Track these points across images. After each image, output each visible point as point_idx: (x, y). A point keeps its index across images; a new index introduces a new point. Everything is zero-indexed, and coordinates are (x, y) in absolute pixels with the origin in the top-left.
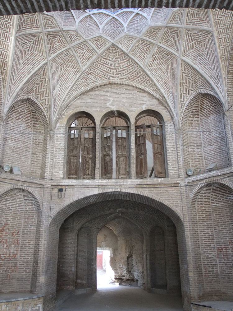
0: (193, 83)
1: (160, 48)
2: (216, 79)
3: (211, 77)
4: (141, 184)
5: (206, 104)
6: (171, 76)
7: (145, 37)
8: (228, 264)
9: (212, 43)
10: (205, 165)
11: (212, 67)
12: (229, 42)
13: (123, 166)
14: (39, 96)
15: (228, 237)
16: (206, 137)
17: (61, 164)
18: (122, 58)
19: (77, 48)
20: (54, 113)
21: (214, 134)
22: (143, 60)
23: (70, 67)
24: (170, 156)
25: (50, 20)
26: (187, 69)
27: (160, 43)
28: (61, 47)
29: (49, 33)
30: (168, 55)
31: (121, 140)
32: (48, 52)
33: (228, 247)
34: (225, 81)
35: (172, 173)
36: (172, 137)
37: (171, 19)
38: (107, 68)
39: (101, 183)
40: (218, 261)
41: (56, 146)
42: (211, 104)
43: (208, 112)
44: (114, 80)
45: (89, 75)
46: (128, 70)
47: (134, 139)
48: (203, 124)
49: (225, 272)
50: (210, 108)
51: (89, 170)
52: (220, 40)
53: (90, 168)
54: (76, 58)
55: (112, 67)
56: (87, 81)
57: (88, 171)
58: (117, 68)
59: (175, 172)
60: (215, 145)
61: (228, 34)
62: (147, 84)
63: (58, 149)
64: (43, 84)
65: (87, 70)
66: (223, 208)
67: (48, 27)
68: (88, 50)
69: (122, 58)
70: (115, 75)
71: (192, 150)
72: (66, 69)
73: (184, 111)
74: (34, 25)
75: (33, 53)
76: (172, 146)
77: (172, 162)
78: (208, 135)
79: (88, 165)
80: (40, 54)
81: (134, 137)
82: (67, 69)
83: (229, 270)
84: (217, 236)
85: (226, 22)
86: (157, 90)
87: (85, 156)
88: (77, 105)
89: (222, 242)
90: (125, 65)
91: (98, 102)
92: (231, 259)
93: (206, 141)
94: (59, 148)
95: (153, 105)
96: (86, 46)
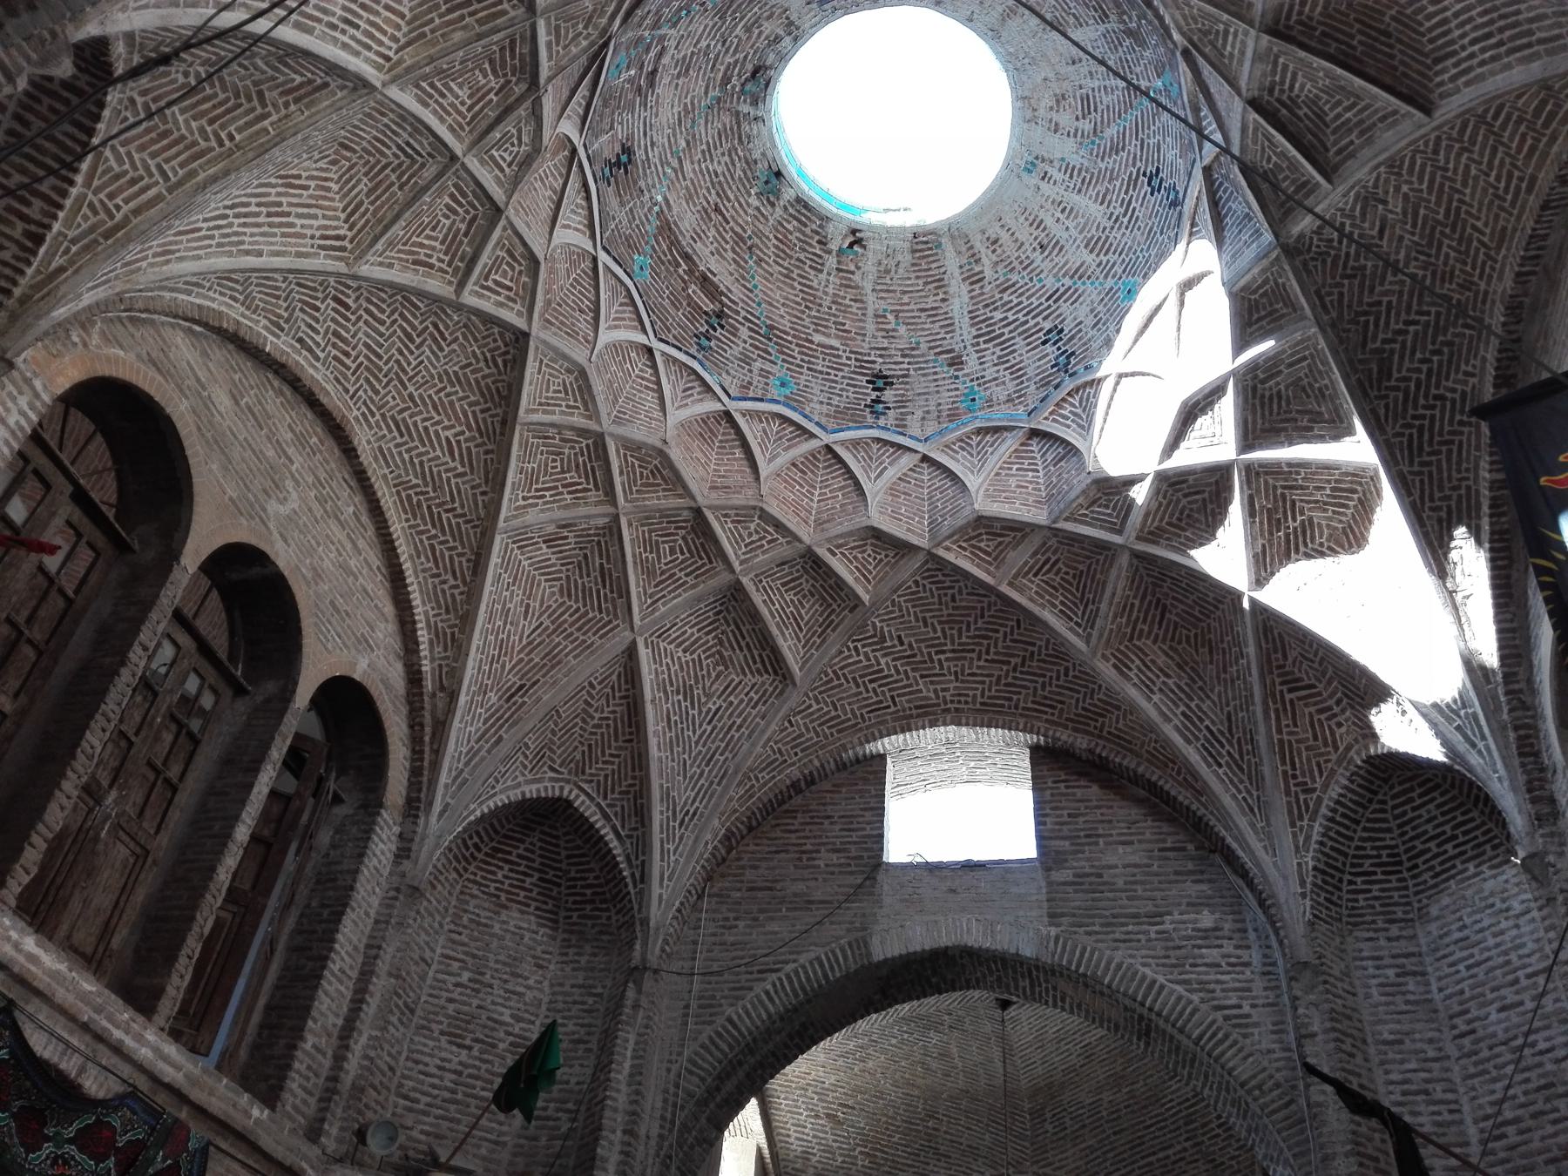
0: (580, 749)
3: (666, 796)
7: (618, 451)
9: (756, 704)
21: (493, 1003)
22: (524, 498)
25: (586, 27)
27: (630, 525)
28: (449, 114)
30: (604, 581)
34: (701, 855)
37: (732, 512)
38: (397, 361)
39: (32, 958)
43: (511, 885)
45: (333, 304)
46: (438, 458)
55: (410, 380)
58: (416, 405)
60: (475, 1052)
61: (818, 735)
62: (437, 580)
64: (229, 111)
67: (557, 28)
68: (455, 237)
70: (378, 417)
72: (326, 179)
80: (405, 29)
82: (331, 185)
86: (455, 643)
88: (167, 357)
90: (449, 433)
93: (443, 1008)
96: (474, 219)
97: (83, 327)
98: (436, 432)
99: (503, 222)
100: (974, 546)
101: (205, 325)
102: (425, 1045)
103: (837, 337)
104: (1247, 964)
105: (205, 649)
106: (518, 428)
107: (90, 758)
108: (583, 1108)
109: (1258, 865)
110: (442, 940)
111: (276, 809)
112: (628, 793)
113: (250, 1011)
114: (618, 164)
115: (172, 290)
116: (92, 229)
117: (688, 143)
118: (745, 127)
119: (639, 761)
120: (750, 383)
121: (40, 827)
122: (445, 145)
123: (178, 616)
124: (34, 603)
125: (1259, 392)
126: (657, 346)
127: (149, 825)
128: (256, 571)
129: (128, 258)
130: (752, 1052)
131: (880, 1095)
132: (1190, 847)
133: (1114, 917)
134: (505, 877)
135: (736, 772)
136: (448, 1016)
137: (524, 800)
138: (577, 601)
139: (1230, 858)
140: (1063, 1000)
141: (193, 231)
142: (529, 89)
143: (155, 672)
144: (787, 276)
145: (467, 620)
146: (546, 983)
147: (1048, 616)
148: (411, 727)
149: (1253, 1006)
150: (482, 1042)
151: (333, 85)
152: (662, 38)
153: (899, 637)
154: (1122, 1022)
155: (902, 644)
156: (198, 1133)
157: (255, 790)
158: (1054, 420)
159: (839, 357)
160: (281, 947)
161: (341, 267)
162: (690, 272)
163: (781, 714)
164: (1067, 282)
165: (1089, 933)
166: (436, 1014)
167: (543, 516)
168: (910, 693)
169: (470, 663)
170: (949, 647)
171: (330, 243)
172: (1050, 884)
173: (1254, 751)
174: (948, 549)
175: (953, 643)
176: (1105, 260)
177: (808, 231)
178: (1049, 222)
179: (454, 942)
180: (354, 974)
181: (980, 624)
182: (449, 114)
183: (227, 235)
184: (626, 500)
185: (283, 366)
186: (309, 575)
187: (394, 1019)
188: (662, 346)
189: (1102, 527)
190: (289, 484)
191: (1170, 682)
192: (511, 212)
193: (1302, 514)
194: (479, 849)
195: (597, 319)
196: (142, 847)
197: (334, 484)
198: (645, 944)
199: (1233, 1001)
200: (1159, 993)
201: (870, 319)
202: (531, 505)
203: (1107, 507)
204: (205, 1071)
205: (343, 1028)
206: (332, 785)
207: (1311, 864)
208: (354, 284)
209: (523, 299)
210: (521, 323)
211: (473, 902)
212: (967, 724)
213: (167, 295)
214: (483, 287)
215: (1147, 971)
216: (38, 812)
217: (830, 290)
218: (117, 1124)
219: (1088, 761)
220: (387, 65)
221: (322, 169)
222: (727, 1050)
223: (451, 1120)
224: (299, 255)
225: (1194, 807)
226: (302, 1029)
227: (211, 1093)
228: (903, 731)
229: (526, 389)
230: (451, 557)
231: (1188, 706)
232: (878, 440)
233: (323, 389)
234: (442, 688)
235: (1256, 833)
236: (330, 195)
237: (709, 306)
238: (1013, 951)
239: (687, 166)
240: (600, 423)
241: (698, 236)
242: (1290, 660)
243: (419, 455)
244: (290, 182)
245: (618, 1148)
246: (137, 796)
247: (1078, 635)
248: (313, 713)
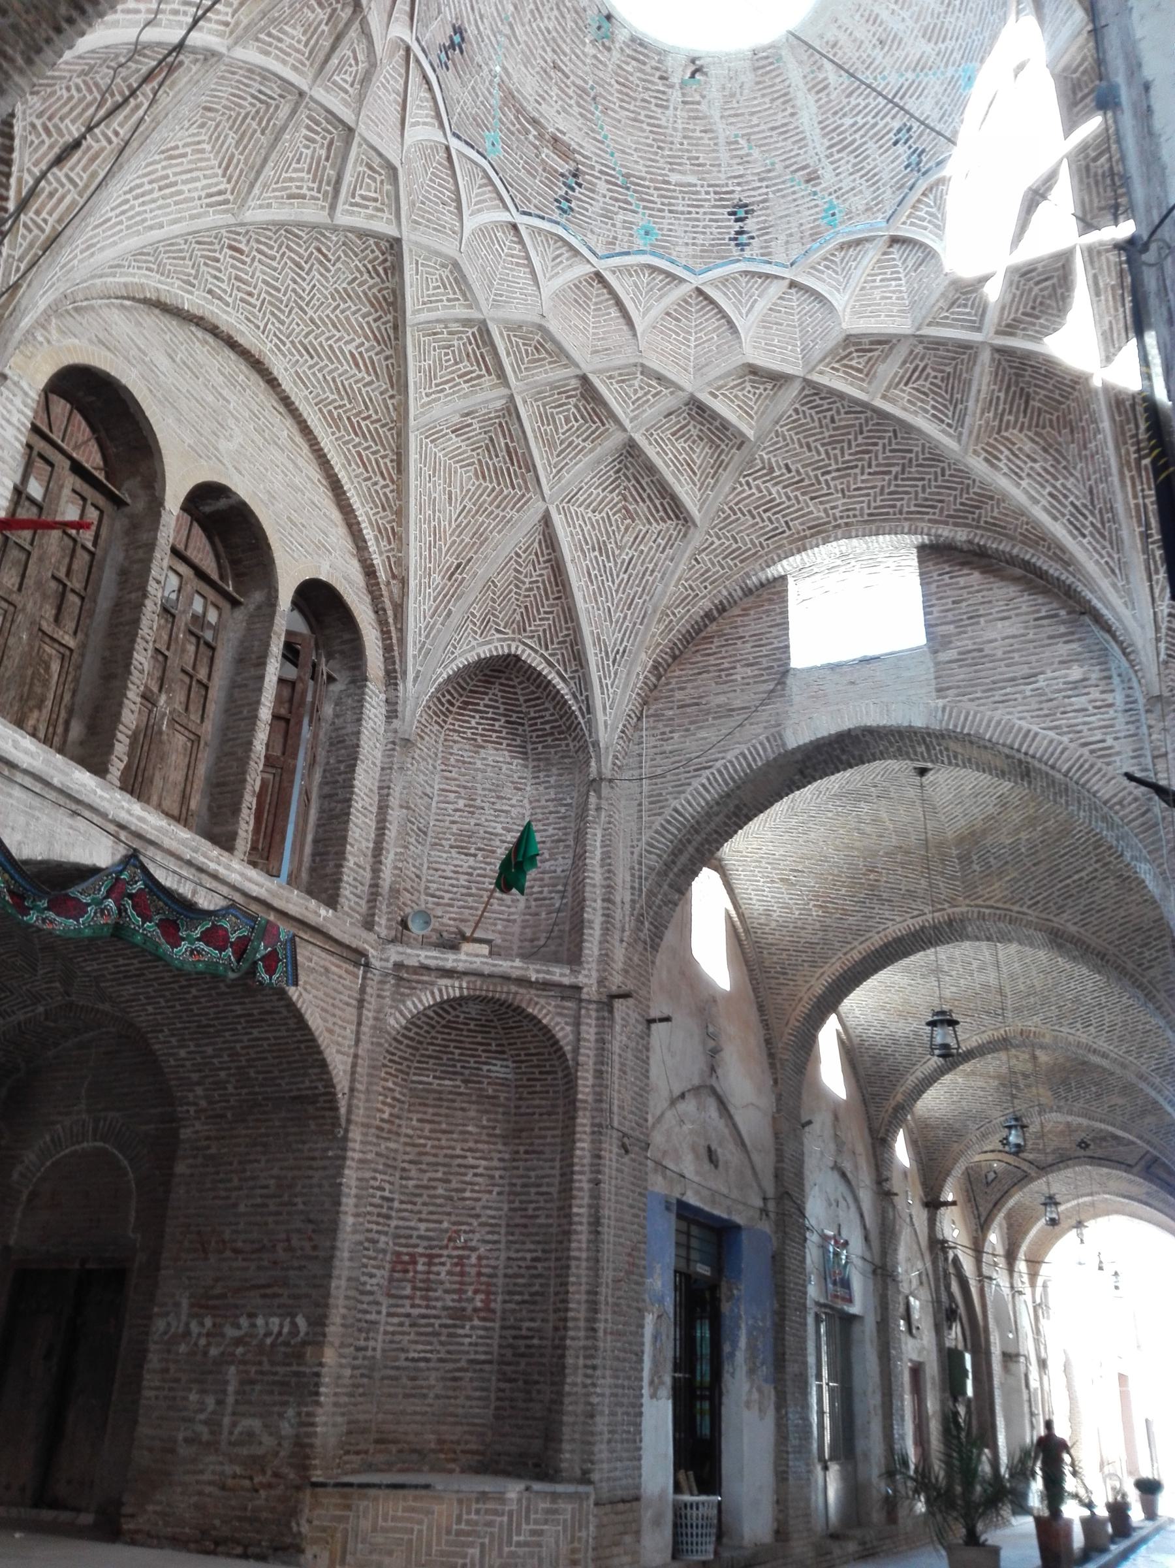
4: (270, 900)
7: (501, 334)
8: (423, 1321)
14: (48, 142)
15: (449, 1214)
18: (369, 314)
22: (427, 395)
23: (218, 152)
27: (525, 402)
28: (289, 55)
33: (440, 1256)
37: (616, 373)
38: (294, 290)
39: (140, 819)
40: (384, 1311)
45: (230, 252)
49: (403, 1356)
53: (49, 703)
57: (36, 714)
60: (480, 858)
62: (369, 483)
66: (454, 1101)
69: (369, 314)
70: (289, 345)
72: (199, 143)
79: (45, 684)
83: (420, 1347)
84: (404, 1206)
86: (396, 536)
89: (422, 1233)
90: (351, 347)
92: (439, 1304)
96: (331, 143)
97: (43, 327)
98: (340, 348)
99: (357, 139)
100: (846, 366)
101: (133, 299)
103: (693, 172)
104: (1110, 705)
105: (200, 574)
106: (408, 329)
107: (142, 672)
108: (569, 888)
109: (1119, 620)
110: (437, 778)
111: (286, 693)
113: (302, 845)
114: (453, 46)
115: (101, 276)
117: (516, 8)
119: (570, 614)
120: (615, 238)
121: (121, 727)
122: (292, 85)
123: (175, 552)
124: (67, 560)
125: (1092, 171)
126: (520, 220)
127: (195, 717)
128: (222, 504)
129: (63, 261)
130: (697, 832)
131: (825, 859)
132: (1063, 613)
133: (994, 682)
135: (654, 611)
137: (480, 661)
139: (1097, 618)
140: (956, 757)
141: (105, 222)
142: (354, 12)
143: (168, 599)
144: (635, 120)
145: (401, 514)
146: (526, 801)
147: (921, 422)
148: (376, 612)
149: (1116, 739)
151: (187, 62)
153: (787, 466)
154: (1006, 769)
155: (789, 471)
156: (285, 930)
157: (267, 679)
158: (912, 224)
159: (697, 193)
160: (314, 796)
161: (229, 219)
162: (540, 136)
163: (687, 555)
164: (910, 76)
165: (972, 700)
167: (448, 409)
168: (803, 516)
169: (412, 552)
170: (834, 467)
171: (217, 200)
172: (937, 664)
173: (1114, 520)
174: (821, 373)
175: (837, 463)
176: (943, 47)
177: (647, 68)
178: (885, 15)
180: (374, 809)
181: (860, 440)
182: (289, 55)
183: (132, 217)
184: (517, 379)
185: (202, 318)
186: (265, 498)
187: (412, 840)
188: (526, 219)
189: (963, 327)
190: (231, 422)
191: (1037, 466)
192: (362, 129)
194: (452, 705)
195: (459, 208)
197: (266, 413)
198: (599, 761)
199: (1099, 737)
200: (1033, 740)
201: (723, 148)
202: (435, 400)
203: (965, 306)
204: (280, 886)
205: (375, 849)
206: (324, 668)
207: (1166, 611)
208: (242, 230)
209: (389, 206)
210: (392, 231)
211: (456, 746)
213: (98, 281)
214: (352, 205)
215: (1023, 723)
216: (116, 718)
217: (679, 126)
218: (227, 926)
219: (969, 551)
220: (228, 30)
221: (194, 135)
222: (676, 832)
223: (471, 908)
224: (192, 217)
225: (1063, 577)
226: (344, 853)
227: (288, 901)
228: (799, 552)
229: (409, 292)
231: (1054, 487)
232: (746, 273)
233: (238, 330)
234: (394, 577)
235: (1117, 591)
236: (206, 156)
237: (564, 167)
238: (906, 724)
239: (519, 30)
241: (542, 99)
243: (330, 372)
244: (170, 154)
245: (600, 912)
246: (180, 696)
247: (950, 435)
248: (296, 613)
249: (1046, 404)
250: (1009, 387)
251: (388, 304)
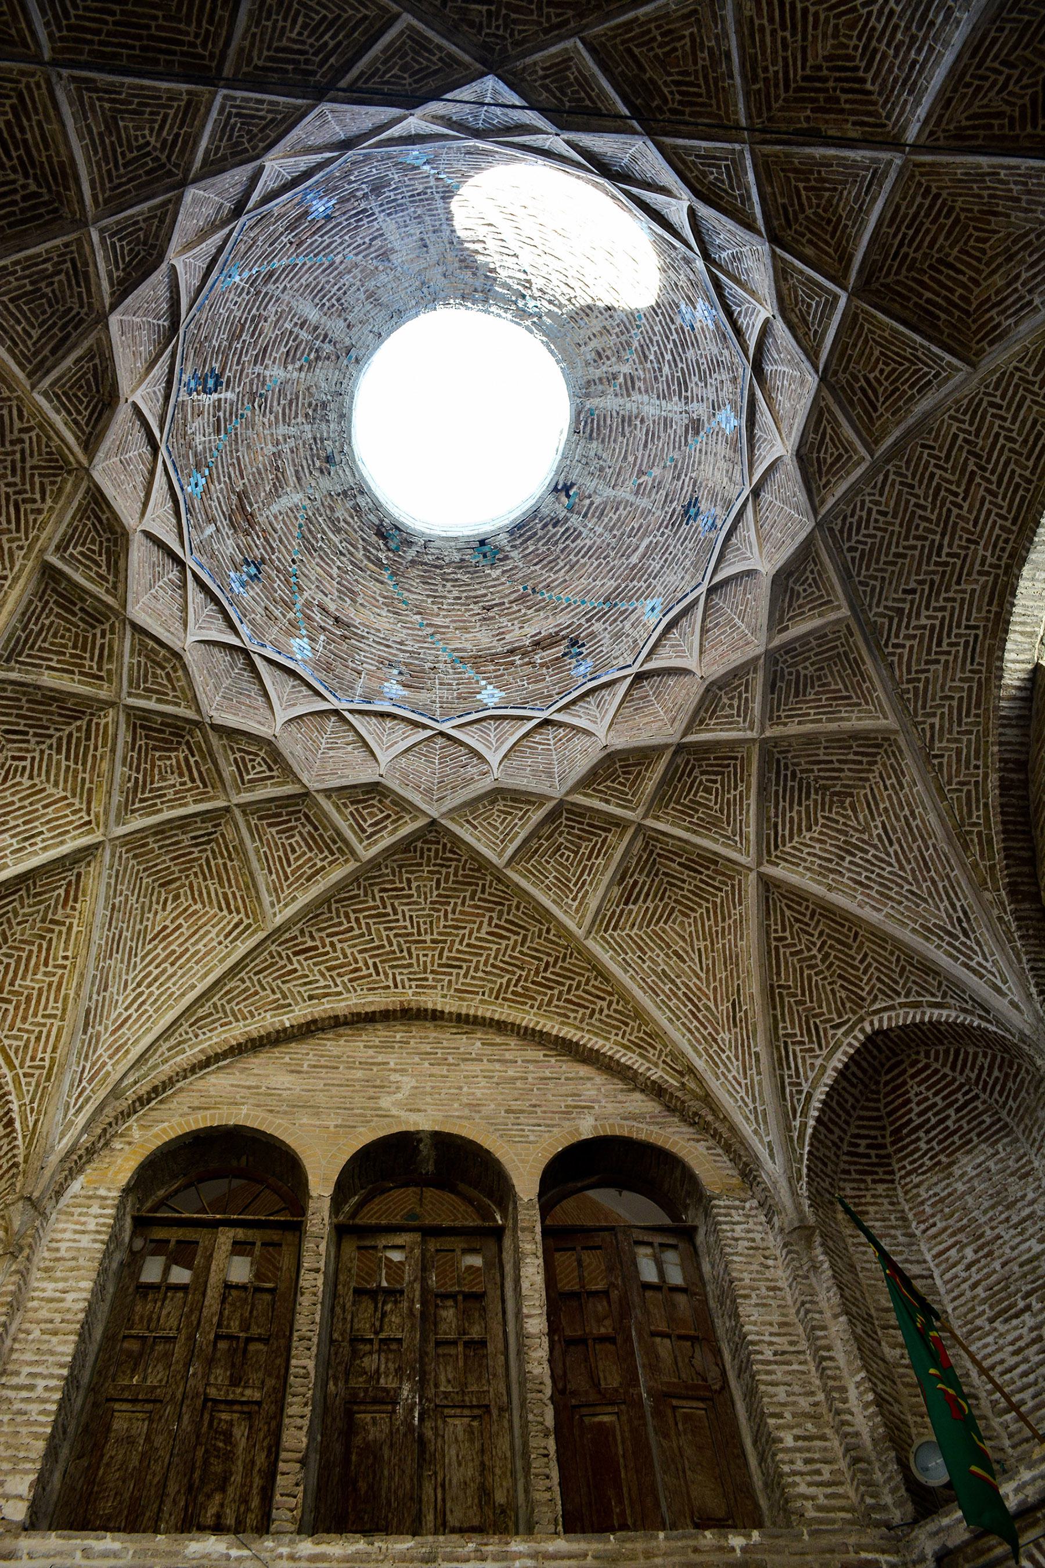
0: (836, 987)
1: (657, 840)
2: (957, 938)
3: (927, 932)
5: (918, 1104)
6: (719, 965)
7: (586, 795)
10: (1010, 1451)
11: (920, 887)
12: (980, 763)
13: (470, 1471)
16: (964, 1274)
17: (36, 1423)
18: (474, 892)
19: (260, 818)
20: (72, 1111)
21: (1013, 1249)
24: (773, 1384)
25: (163, 668)
26: (797, 920)
29: (145, 719)
31: (452, 1311)
32: (117, 798)
35: (813, 1498)
36: (768, 1275)
37: (702, 713)
38: (396, 935)
41: (35, 1304)
42: (944, 1099)
43: (939, 1143)
44: (423, 998)
45: (301, 957)
47: (539, 1279)
48: (929, 1210)
50: (948, 1117)
51: (223, 1490)
52: (936, 761)
53: (237, 1478)
54: (247, 860)
56: (284, 987)
57: (218, 1498)
59: (829, 1490)
61: (970, 732)
63: (38, 1322)
64: (48, 949)
65: (295, 931)
67: (146, 690)
69: (474, 892)
70: (430, 977)
71: (902, 1357)
73: (810, 1131)
74: (87, 663)
75: (43, 790)
76: (775, 1329)
77: (799, 1425)
78: (978, 1261)
79: (228, 1457)
80: (77, 801)
81: (541, 1270)
85: (949, 684)
87: (213, 1392)
90: (485, 928)
91: (334, 1090)
93: (974, 1298)
94: (51, 1321)
95: (634, 1117)
99: (321, 799)
102: (986, 1346)
103: (641, 539)
106: (509, 872)
112: (903, 968)
116: (37, 1085)
118: (427, 559)
134: (928, 1142)
136: (984, 1301)
138: (700, 906)
148: (693, 1124)
150: (1034, 1291)
152: (308, 604)
153: (905, 591)
166: (973, 1309)
168: (971, 604)
170: (938, 537)
175: (935, 533)
177: (540, 533)
179: (935, 1237)
184: (634, 810)
189: (829, 318)
193: (819, 68)
196: (478, 1407)
202: (584, 897)
211: (922, 1190)
212: (1028, 551)
214: (368, 837)
228: (1006, 631)
230: (585, 991)
237: (561, 649)
239: (438, 621)
240: (552, 798)
241: (500, 635)
242: (1007, 109)
243: (486, 964)
247: (947, 379)
249: (957, 241)
250: (921, 283)
251: (478, 870)
